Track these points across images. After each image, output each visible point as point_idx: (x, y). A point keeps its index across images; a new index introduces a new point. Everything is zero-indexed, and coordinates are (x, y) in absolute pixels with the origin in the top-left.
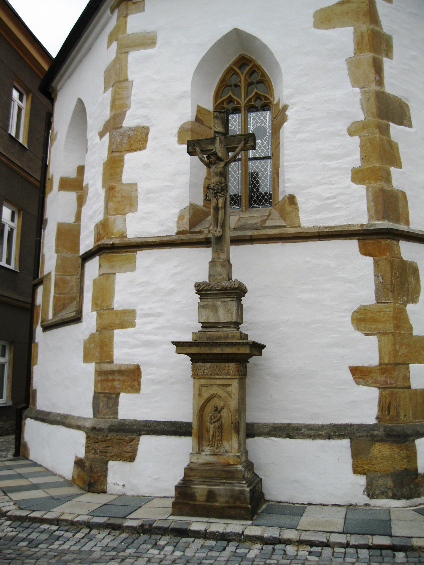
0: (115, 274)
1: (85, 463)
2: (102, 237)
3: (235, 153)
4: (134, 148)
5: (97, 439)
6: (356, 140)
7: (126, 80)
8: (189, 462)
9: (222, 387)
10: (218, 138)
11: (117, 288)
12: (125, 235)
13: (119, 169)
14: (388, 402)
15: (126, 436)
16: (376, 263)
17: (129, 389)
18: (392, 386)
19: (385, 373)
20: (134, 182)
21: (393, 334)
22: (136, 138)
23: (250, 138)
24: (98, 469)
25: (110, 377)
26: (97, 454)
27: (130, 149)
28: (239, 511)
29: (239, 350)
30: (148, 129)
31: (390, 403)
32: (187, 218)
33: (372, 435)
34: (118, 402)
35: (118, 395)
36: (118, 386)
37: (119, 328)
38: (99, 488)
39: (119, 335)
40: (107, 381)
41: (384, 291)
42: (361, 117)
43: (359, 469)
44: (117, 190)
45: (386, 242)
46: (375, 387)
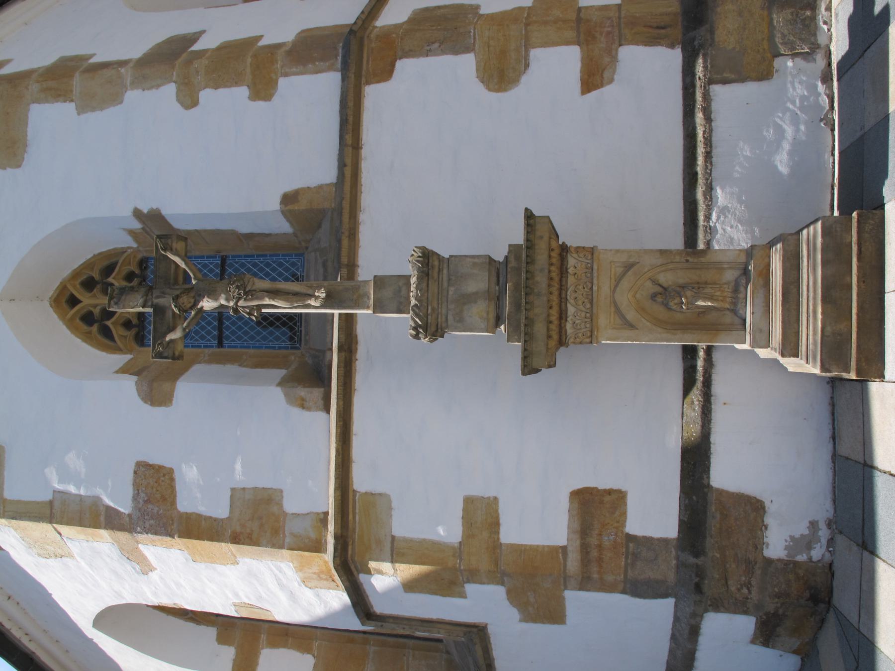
0: (393, 537)
1: (767, 614)
2: (324, 568)
6: (206, 95)
7: (51, 503)
10: (156, 301)
13: (203, 522)
17: (617, 513)
21: (527, 25)
22: (152, 488)
25: (594, 553)
26: (750, 583)
28: (867, 235)
29: (541, 237)
30: (139, 464)
31: (645, 26)
32: (302, 392)
34: (644, 537)
35: (630, 538)
36: (612, 538)
37: (498, 533)
39: (511, 533)
42: (170, 90)
44: (238, 529)
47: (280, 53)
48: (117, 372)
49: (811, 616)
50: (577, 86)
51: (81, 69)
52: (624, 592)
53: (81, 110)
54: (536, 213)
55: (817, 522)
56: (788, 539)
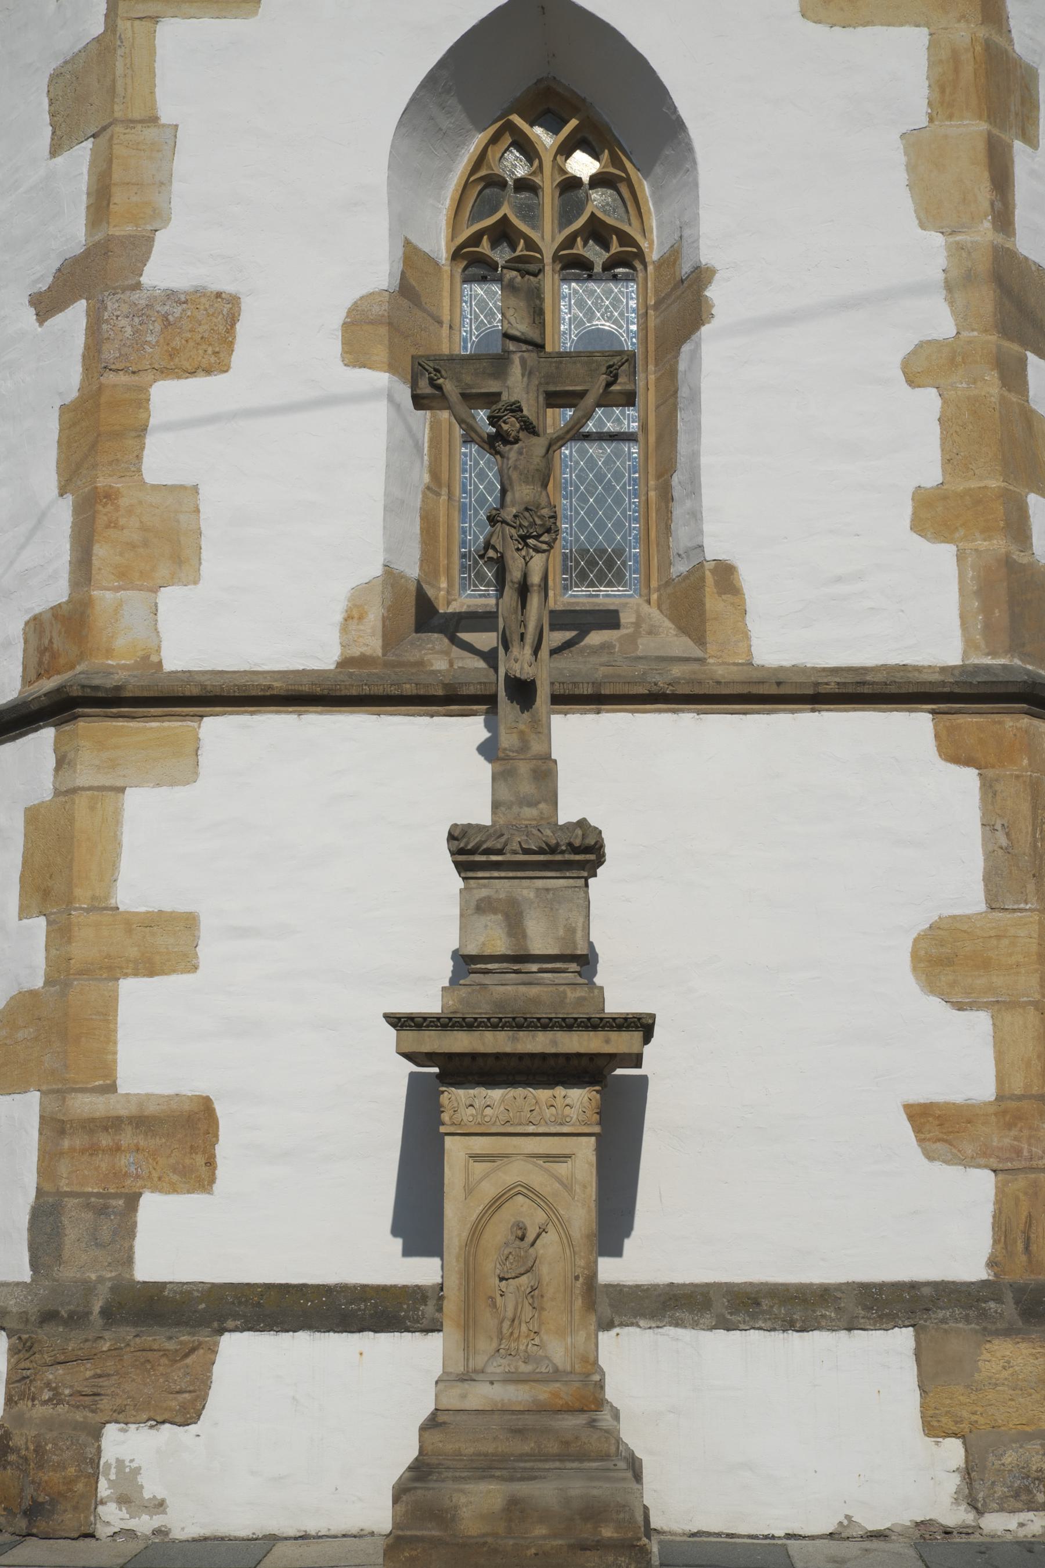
0: (122, 790)
2: (62, 661)
3: (580, 413)
4: (187, 365)
5: (64, 1351)
6: (928, 401)
8: (433, 1407)
9: (541, 1162)
10: (516, 358)
11: (129, 836)
12: (154, 658)
14: (1025, 1213)
15: (170, 1338)
16: (988, 787)
17: (175, 1178)
18: (1034, 1163)
19: (1015, 1125)
20: (188, 481)
23: (625, 367)
24: (67, 1454)
25: (105, 1140)
27: (172, 365)
30: (234, 301)
31: (1030, 1215)
32: (374, 616)
35: (132, 1201)
36: (133, 1169)
37: (136, 974)
38: (68, 1519)
39: (137, 998)
40: (91, 1155)
41: (1011, 873)
42: (942, 324)
43: (944, 1420)
44: (124, 502)
45: (1018, 725)
46: (986, 1167)
48: (407, 243)
51: (996, 131)
52: (40, 1192)
53: (912, 140)
55: (164, 1512)
56: (134, 1465)
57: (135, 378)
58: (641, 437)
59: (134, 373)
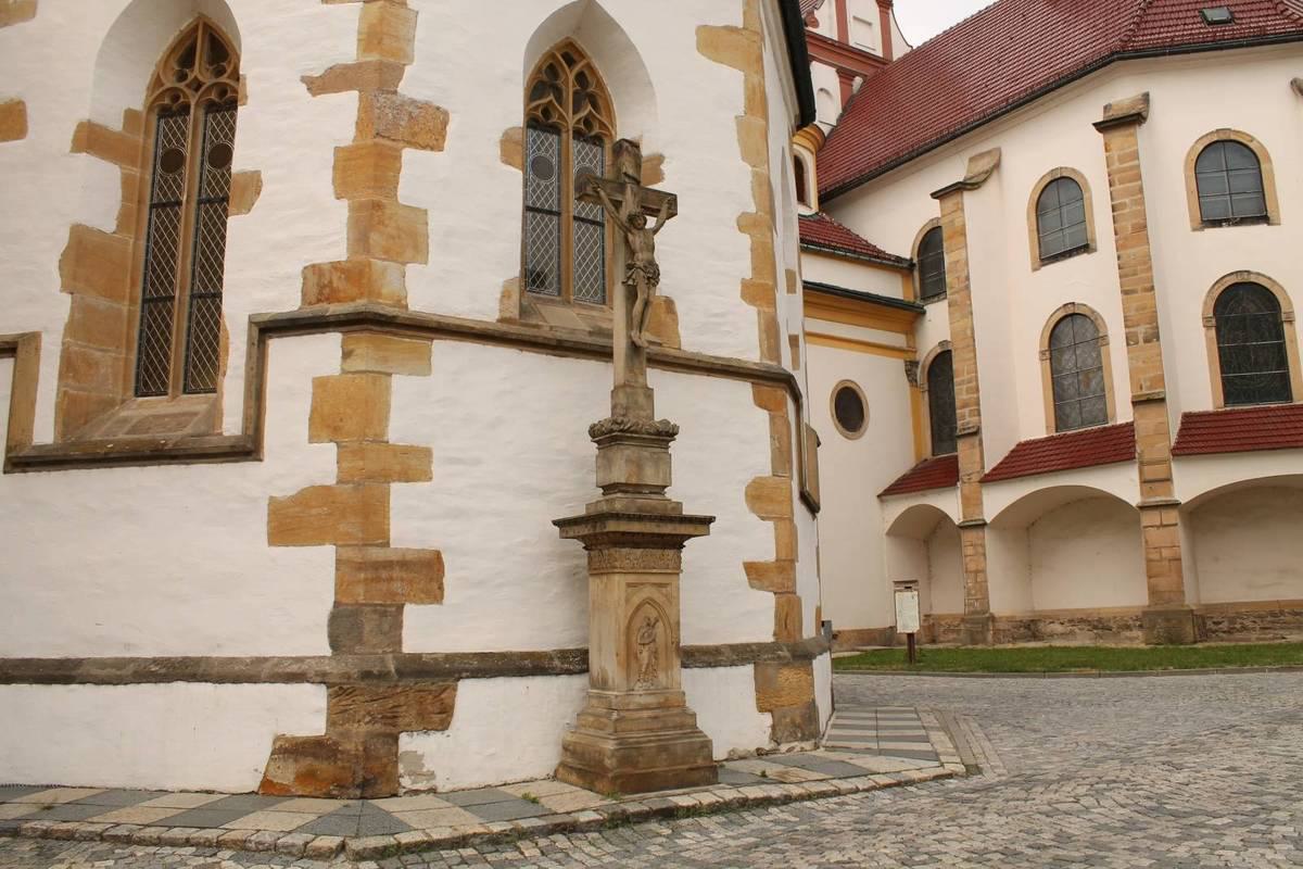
0: (390, 375)
5: (377, 694)
10: (629, 185)
11: (395, 401)
13: (392, 174)
15: (433, 684)
16: (772, 419)
17: (422, 596)
20: (423, 206)
25: (384, 574)
26: (376, 722)
27: (413, 140)
33: (779, 657)
35: (400, 608)
36: (400, 590)
37: (400, 481)
44: (388, 211)
47: (771, 310)
49: (933, 624)
50: (748, 559)
54: (712, 525)
57: (394, 143)
58: (571, 219)
59: (394, 140)
